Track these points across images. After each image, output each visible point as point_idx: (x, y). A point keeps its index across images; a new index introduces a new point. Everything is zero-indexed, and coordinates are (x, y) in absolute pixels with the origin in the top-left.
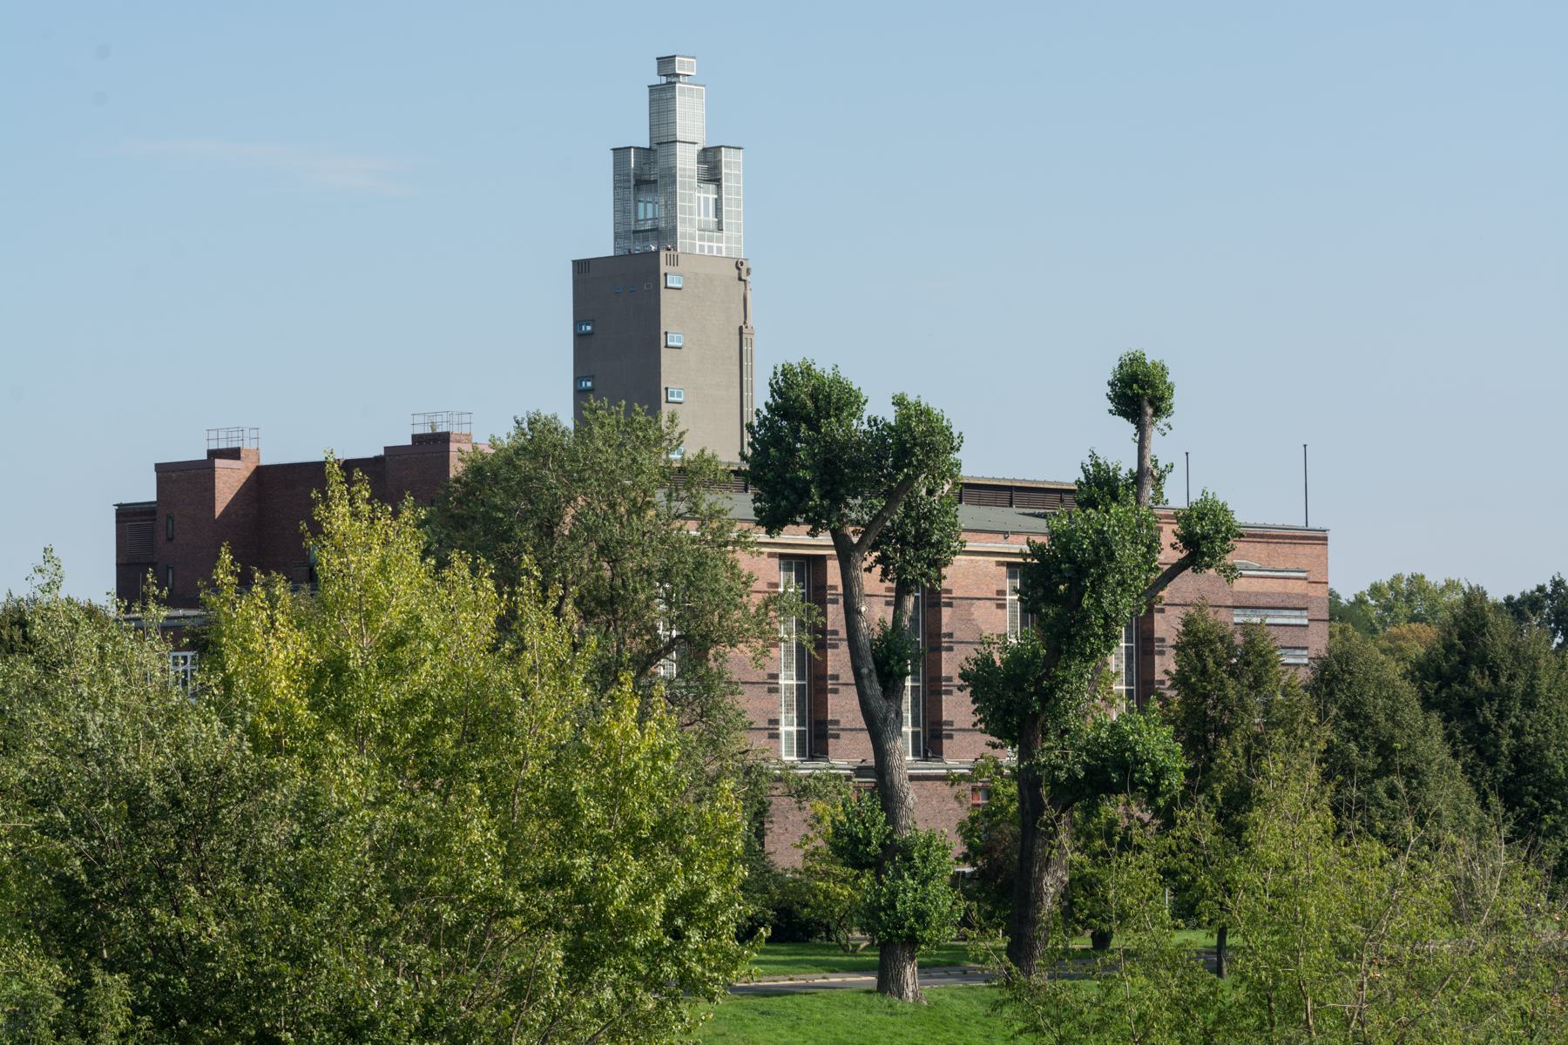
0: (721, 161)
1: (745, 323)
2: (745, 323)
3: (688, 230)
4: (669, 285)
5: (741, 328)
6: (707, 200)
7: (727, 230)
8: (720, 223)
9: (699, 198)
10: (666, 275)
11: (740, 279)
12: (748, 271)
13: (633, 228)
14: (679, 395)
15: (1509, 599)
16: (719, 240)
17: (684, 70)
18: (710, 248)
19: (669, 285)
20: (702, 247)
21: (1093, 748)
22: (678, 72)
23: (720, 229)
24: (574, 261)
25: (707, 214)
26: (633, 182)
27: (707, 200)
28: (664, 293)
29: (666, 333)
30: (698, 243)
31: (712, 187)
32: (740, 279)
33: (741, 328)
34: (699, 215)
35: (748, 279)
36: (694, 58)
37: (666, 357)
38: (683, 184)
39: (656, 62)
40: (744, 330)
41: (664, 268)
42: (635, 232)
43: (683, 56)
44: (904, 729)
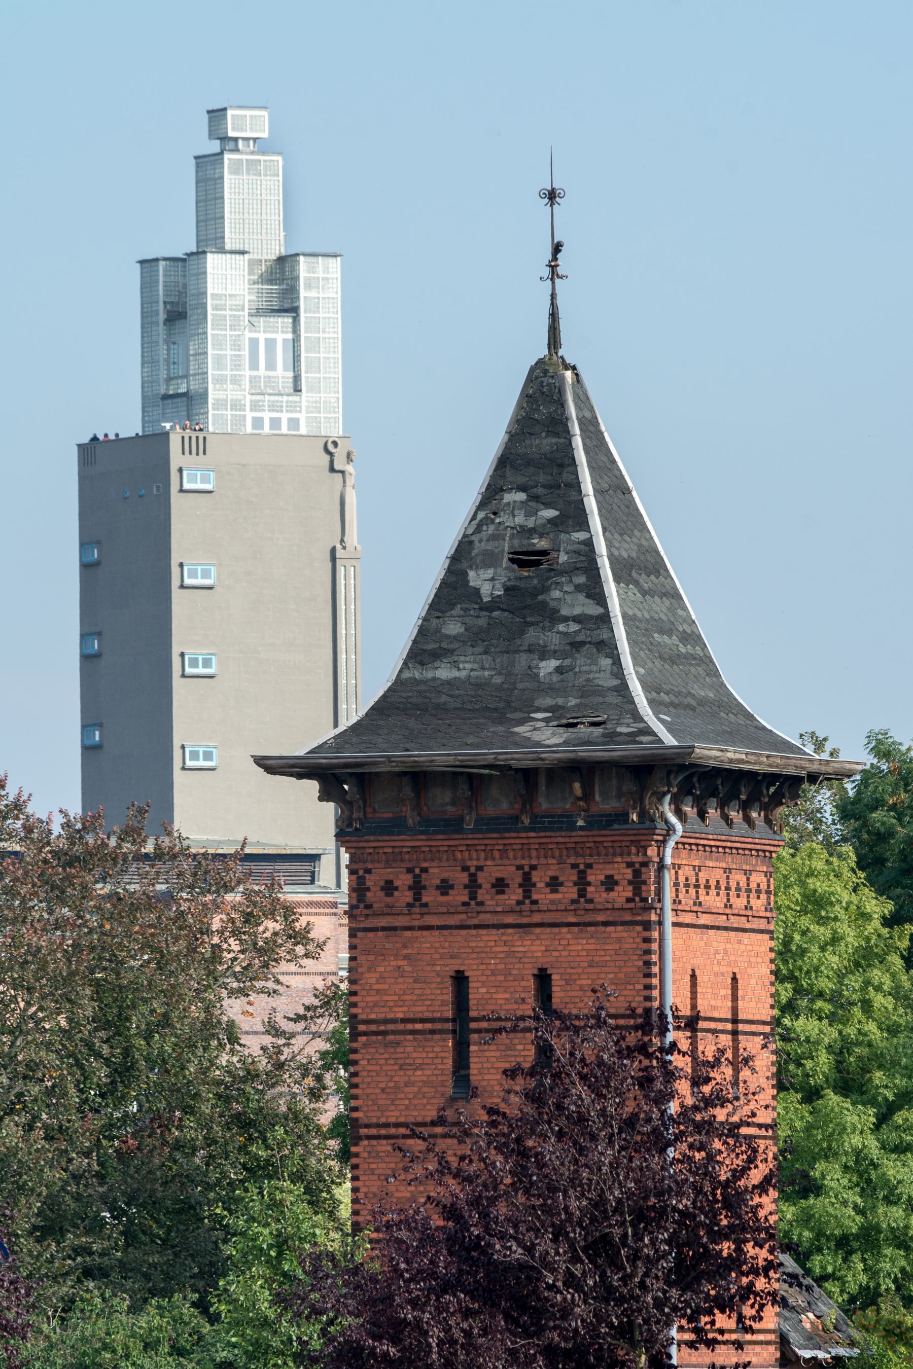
0: (297, 278)
1: (342, 541)
2: (342, 541)
3: (231, 393)
4: (186, 486)
5: (333, 551)
6: (271, 344)
7: (307, 392)
8: (297, 379)
9: (254, 343)
10: (180, 470)
11: (332, 469)
12: (349, 457)
13: (163, 391)
14: (207, 663)
15: (325, 796)
16: (294, 407)
17: (242, 130)
18: (275, 423)
19: (186, 486)
20: (257, 423)
21: (823, 1184)
22: (231, 134)
23: (297, 390)
24: (79, 446)
25: (271, 366)
26: (162, 316)
27: (271, 344)
28: (177, 501)
29: (181, 565)
30: (249, 415)
31: (286, 321)
32: (332, 469)
33: (333, 551)
34: (254, 366)
35: (349, 468)
36: (265, 108)
37: (180, 602)
38: (220, 322)
39: (205, 118)
40: (340, 553)
41: (176, 458)
42: (166, 397)
43: (240, 107)
44: (352, 1101)
